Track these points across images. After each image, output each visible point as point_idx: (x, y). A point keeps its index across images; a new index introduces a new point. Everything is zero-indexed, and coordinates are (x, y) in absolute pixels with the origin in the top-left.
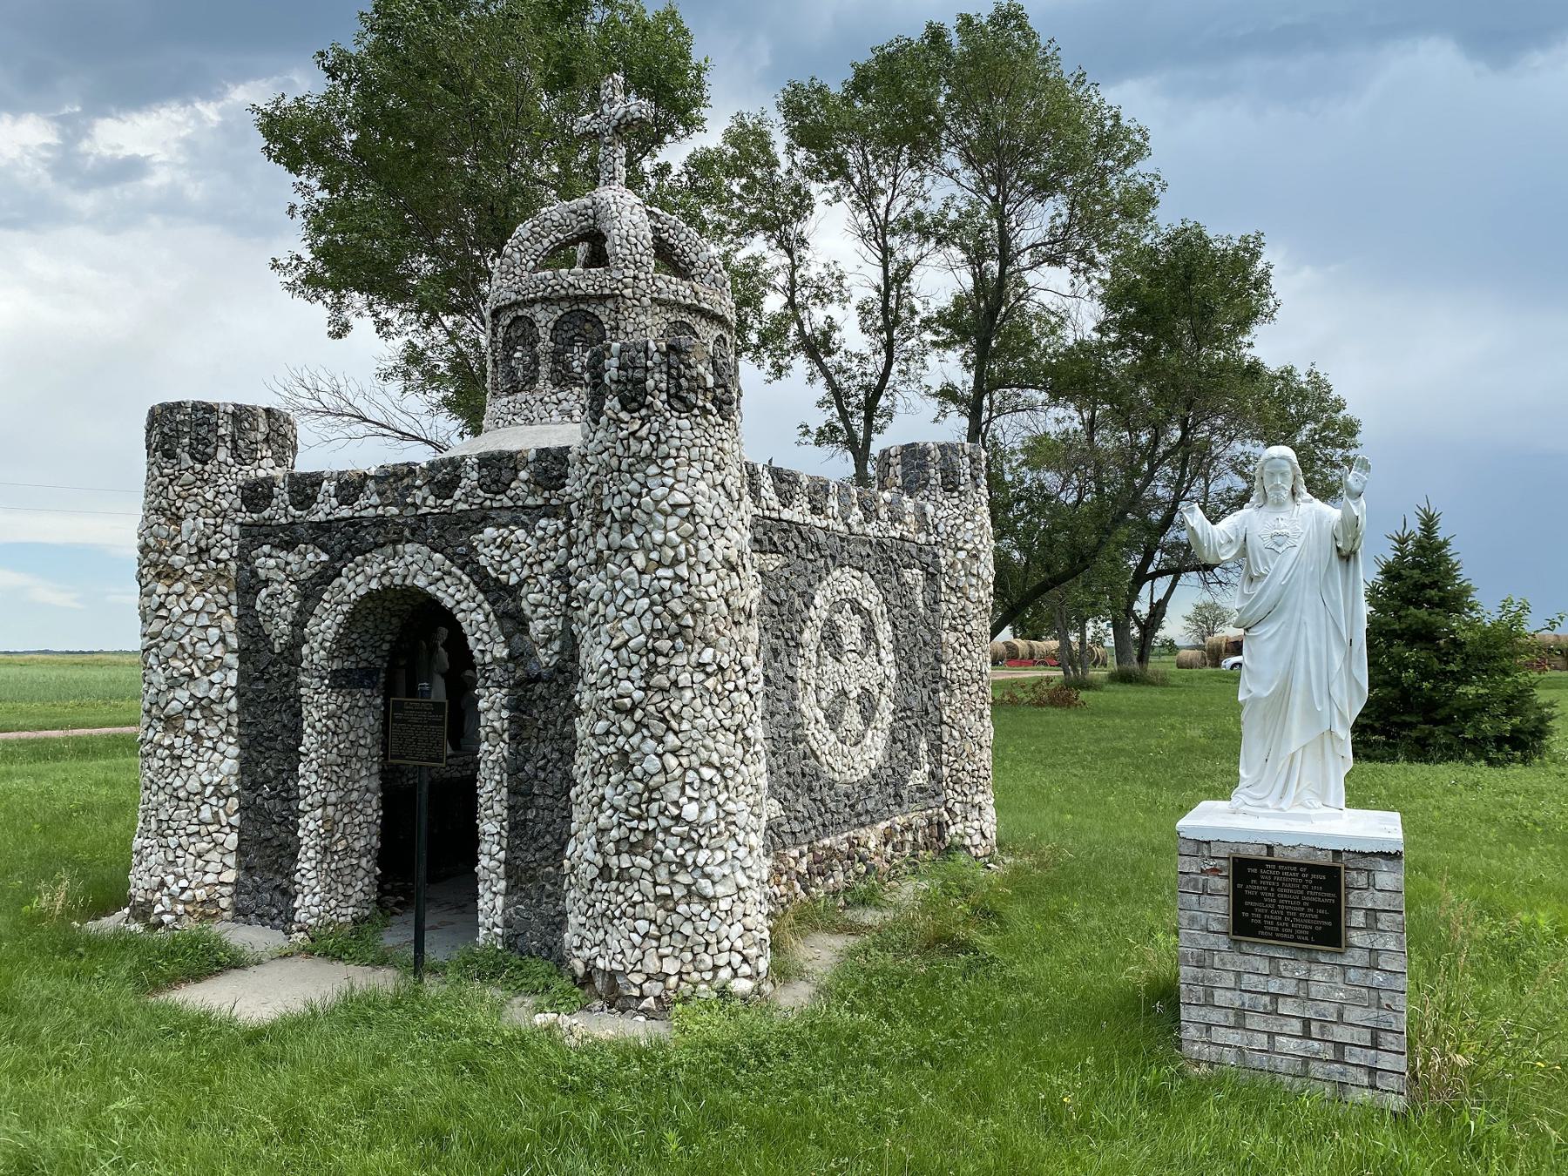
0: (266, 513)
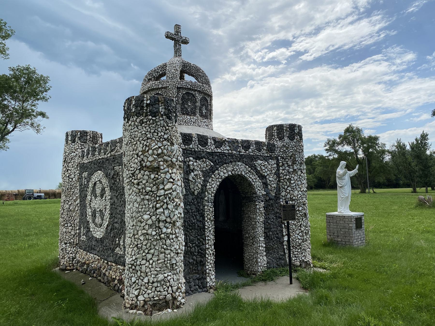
0: (191, 146)
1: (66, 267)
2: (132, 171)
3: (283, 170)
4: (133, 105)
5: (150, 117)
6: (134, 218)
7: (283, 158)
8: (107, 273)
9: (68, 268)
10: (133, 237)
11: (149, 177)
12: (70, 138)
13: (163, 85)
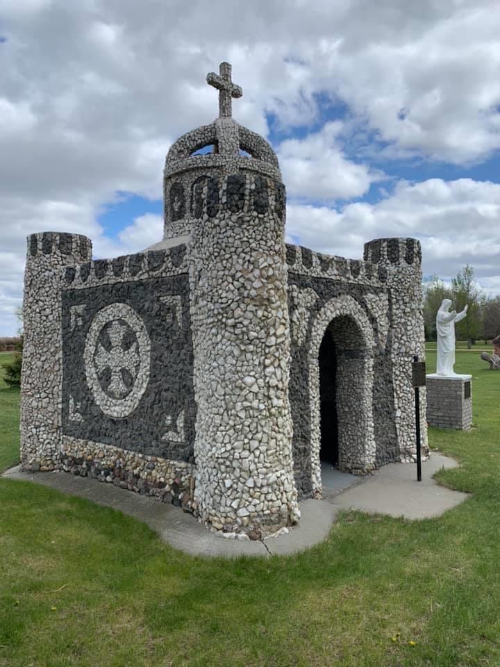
1: (40, 466)
2: (222, 303)
3: (398, 309)
4: (224, 191)
5: (255, 214)
6: (228, 383)
7: (397, 291)
8: (144, 475)
9: (45, 467)
10: (225, 414)
11: (254, 313)
12: (40, 245)
13: (215, 162)
